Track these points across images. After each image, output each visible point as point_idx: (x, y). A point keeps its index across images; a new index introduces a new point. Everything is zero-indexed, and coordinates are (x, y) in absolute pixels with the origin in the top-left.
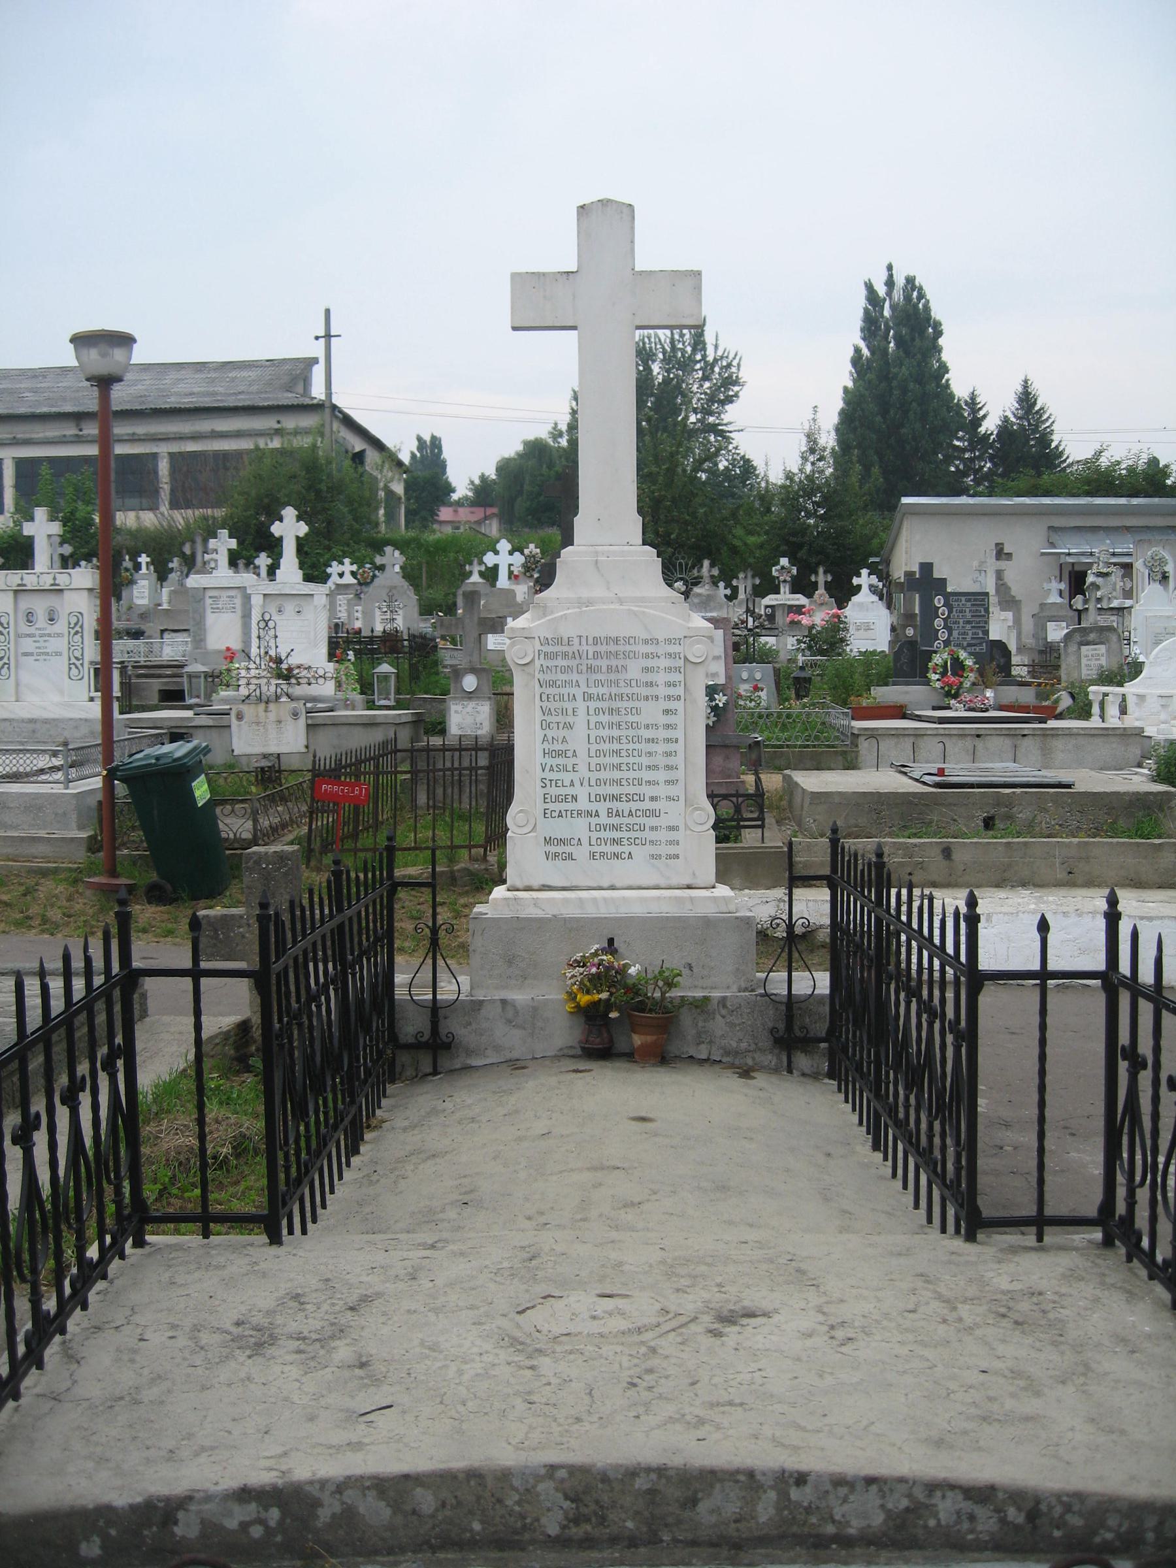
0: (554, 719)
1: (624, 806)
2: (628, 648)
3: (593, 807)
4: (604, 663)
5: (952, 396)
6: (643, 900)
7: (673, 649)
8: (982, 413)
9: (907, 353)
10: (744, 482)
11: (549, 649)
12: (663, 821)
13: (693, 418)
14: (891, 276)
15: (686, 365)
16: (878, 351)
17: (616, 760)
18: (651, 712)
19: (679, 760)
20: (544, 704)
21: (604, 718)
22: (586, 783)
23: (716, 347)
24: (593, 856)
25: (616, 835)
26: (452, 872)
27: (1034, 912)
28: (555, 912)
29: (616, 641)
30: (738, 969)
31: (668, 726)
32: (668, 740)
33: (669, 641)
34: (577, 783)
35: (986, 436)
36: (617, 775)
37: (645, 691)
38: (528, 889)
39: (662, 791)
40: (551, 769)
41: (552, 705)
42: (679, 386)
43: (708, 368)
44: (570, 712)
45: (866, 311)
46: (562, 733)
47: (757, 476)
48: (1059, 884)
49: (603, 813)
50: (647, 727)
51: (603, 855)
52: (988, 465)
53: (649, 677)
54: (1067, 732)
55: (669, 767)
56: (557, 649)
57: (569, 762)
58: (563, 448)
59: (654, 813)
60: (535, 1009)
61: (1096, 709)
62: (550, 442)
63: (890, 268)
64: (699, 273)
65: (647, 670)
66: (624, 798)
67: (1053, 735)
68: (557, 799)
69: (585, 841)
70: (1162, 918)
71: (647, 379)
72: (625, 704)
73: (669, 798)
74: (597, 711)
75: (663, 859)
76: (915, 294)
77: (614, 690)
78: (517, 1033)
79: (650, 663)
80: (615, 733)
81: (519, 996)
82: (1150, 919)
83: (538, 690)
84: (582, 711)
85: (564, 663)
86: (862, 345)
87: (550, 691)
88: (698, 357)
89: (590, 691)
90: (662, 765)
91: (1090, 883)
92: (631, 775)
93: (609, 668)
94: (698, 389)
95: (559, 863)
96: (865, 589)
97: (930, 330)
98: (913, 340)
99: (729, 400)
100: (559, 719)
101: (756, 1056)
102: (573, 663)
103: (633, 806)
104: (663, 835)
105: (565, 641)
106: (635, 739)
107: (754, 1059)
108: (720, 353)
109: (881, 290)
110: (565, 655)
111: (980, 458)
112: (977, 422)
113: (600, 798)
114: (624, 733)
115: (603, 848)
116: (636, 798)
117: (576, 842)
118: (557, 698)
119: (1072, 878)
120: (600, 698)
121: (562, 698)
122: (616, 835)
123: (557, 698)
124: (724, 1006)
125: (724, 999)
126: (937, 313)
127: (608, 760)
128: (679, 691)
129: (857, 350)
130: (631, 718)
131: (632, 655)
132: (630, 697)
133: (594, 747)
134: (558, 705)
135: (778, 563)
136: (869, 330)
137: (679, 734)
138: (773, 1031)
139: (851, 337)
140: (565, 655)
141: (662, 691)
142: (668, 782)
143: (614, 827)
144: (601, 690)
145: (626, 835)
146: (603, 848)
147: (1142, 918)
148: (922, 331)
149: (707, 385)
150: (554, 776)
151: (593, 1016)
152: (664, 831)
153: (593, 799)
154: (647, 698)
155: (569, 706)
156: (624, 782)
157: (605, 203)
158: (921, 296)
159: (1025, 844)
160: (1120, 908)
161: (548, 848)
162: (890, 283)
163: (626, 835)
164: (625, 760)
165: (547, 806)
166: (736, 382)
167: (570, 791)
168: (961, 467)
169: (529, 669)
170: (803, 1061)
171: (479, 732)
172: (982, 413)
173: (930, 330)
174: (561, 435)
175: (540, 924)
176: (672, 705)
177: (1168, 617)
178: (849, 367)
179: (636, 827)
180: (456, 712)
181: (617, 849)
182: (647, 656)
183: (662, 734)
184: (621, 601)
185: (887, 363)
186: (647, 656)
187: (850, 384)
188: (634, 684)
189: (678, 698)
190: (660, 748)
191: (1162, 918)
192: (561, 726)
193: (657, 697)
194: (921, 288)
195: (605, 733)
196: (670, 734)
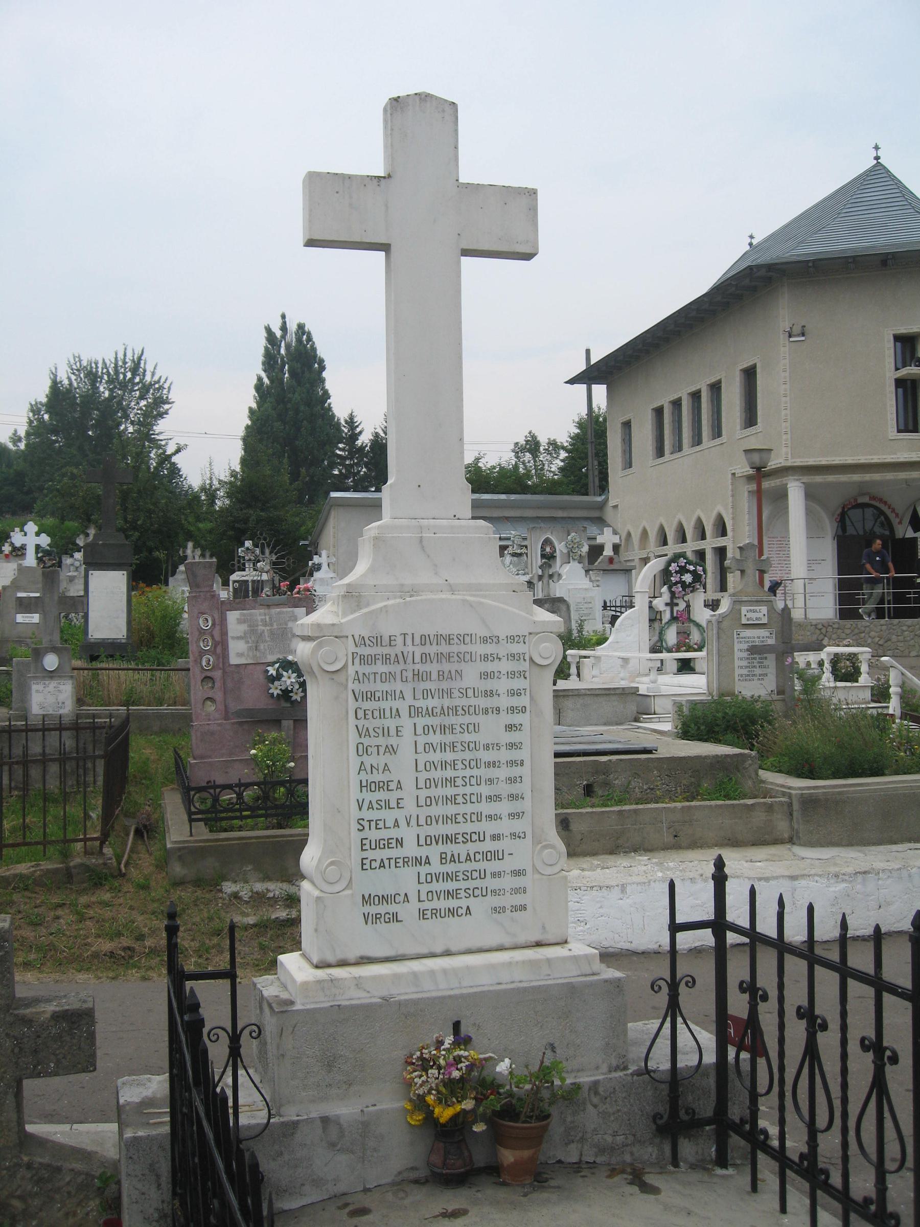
0: (374, 741)
1: (461, 849)
2: (463, 648)
3: (423, 852)
4: (433, 668)
5: (333, 416)
6: (492, 967)
7: (516, 648)
8: (358, 430)
9: (299, 383)
10: (170, 481)
11: (367, 651)
12: (507, 865)
13: (131, 429)
14: (284, 323)
15: (125, 385)
16: (276, 380)
17: (450, 791)
18: (491, 729)
19: (525, 788)
20: (361, 723)
21: (435, 739)
22: (413, 822)
23: (153, 374)
24: (422, 914)
25: (451, 886)
26: (68, 869)
27: (662, 880)
28: (385, 993)
29: (449, 639)
30: (607, 1044)
31: (512, 746)
32: (512, 763)
33: (512, 639)
34: (403, 823)
35: (362, 448)
36: (451, 809)
37: (483, 702)
38: (343, 964)
39: (505, 826)
40: (371, 807)
41: (371, 724)
42: (120, 403)
43: (145, 389)
44: (393, 732)
45: (266, 349)
46: (382, 760)
47: (181, 476)
48: (666, 848)
49: (435, 860)
50: (487, 747)
51: (435, 912)
52: (364, 470)
53: (489, 685)
54: (576, 693)
55: (513, 797)
56: (374, 650)
57: (393, 797)
58: (22, 451)
59: (496, 856)
60: (365, 1125)
61: (573, 670)
62: (11, 446)
63: (283, 317)
64: (533, 193)
65: (485, 675)
66: (461, 839)
67: (564, 696)
68: (379, 845)
69: (413, 897)
70: (776, 878)
71: (94, 393)
72: (460, 720)
73: (514, 835)
74: (427, 729)
75: (508, 912)
76: (305, 337)
77: (447, 702)
78: (343, 1158)
79: (489, 667)
80: (449, 756)
81: (345, 1110)
82: (767, 879)
83: (352, 704)
84: (407, 731)
85: (384, 669)
86: (263, 375)
87: (367, 705)
88: (137, 380)
89: (418, 704)
90: (504, 795)
91: (694, 845)
92: (469, 808)
93: (441, 674)
94: (138, 407)
95: (381, 927)
96: (325, 567)
97: (316, 365)
98: (303, 372)
99: (161, 415)
100: (381, 741)
101: (635, 1150)
102: (396, 669)
103: (472, 847)
104: (508, 882)
105: (386, 640)
106: (473, 763)
107: (632, 1154)
108: (156, 378)
109: (278, 334)
110: (386, 659)
111: (358, 464)
112: (354, 437)
113: (431, 840)
114: (459, 756)
115: (436, 904)
116: (475, 837)
117: (401, 898)
118: (376, 714)
119: (680, 841)
120: (431, 713)
121: (382, 714)
122: (451, 886)
123: (376, 714)
124: (596, 1093)
125: (596, 1083)
126: (321, 352)
127: (440, 792)
128: (524, 701)
129: (260, 379)
130: (467, 737)
131: (468, 657)
132: (466, 711)
133: (423, 776)
134: (378, 723)
135: (243, 545)
136: (269, 363)
137: (523, 754)
138: (656, 1117)
139: (253, 368)
140: (386, 659)
141: (504, 702)
142: (512, 816)
143: (448, 877)
144: (431, 703)
145: (463, 885)
146: (436, 904)
147: (760, 879)
148: (311, 367)
149: (143, 403)
150: (373, 815)
151: (449, 1134)
152: (508, 877)
153: (422, 842)
154: (486, 711)
155: (391, 723)
156: (460, 818)
157: (424, 98)
158: (309, 339)
159: (635, 811)
160: (726, 870)
161: (367, 909)
162: (284, 328)
163: (463, 885)
164: (461, 790)
165: (365, 854)
166: (167, 402)
167: (394, 833)
168: (344, 471)
169: (341, 678)
170: (687, 1149)
171: (62, 711)
172: (358, 430)
173: (316, 365)
174: (20, 440)
175: (366, 1012)
176: (517, 719)
177: (586, 589)
178: (253, 392)
179: (475, 875)
180: (37, 691)
181: (452, 903)
182: (485, 658)
183: (504, 755)
184: (452, 589)
185: (283, 389)
186: (485, 658)
187: (254, 406)
188: (470, 693)
189: (523, 710)
190: (503, 773)
191: (776, 878)
192: (382, 750)
193: (498, 710)
194: (309, 334)
195: (436, 757)
196: (515, 755)
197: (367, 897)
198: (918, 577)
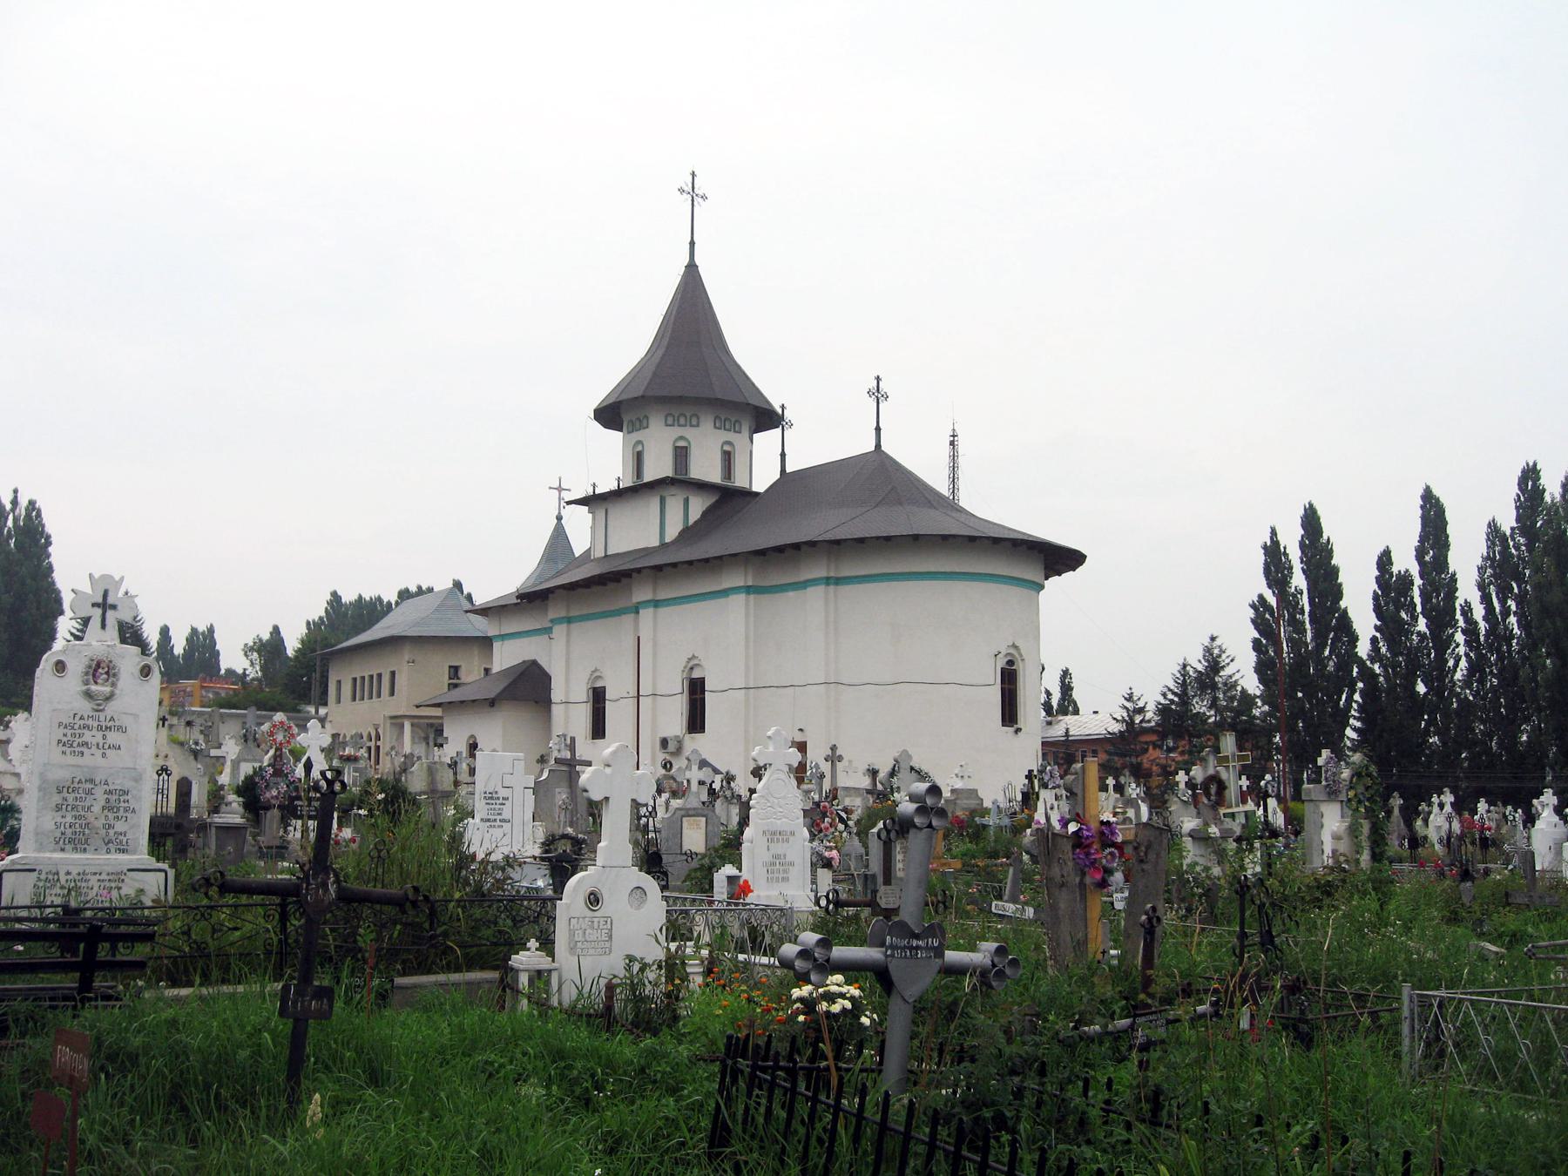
63: (16, 491)
126: (50, 528)
162: (15, 502)
194: (39, 512)
197: (816, 755)
198: (983, 1167)
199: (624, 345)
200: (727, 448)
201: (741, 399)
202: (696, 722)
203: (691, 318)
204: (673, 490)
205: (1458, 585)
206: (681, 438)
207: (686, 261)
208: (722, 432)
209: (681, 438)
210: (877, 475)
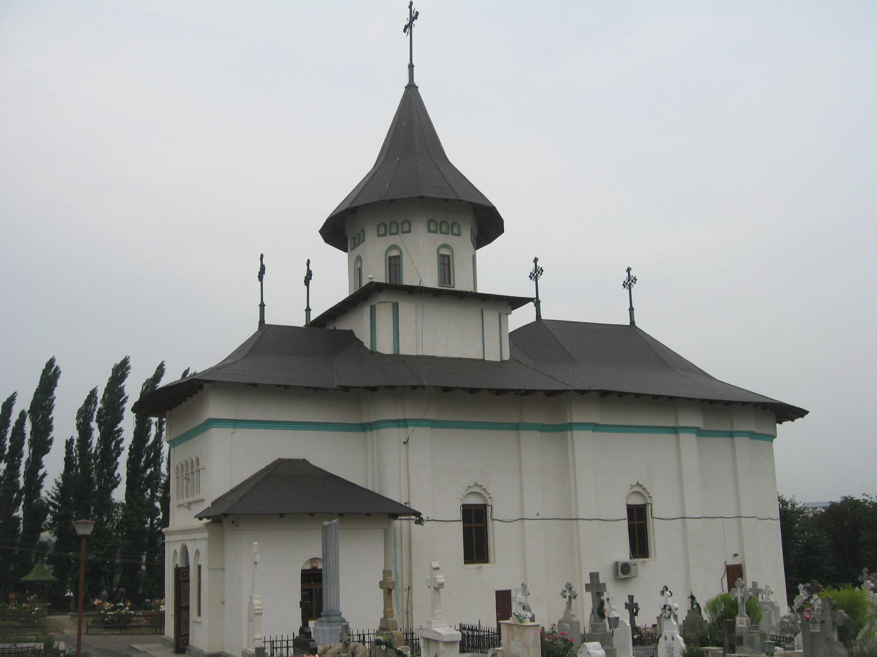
199: (350, 160)
200: (444, 252)
201: (455, 197)
202: (640, 544)
203: (411, 131)
204: (382, 297)
205: (59, 381)
206: (394, 247)
207: (406, 82)
208: (438, 236)
209: (445, 246)
210: (627, 342)
